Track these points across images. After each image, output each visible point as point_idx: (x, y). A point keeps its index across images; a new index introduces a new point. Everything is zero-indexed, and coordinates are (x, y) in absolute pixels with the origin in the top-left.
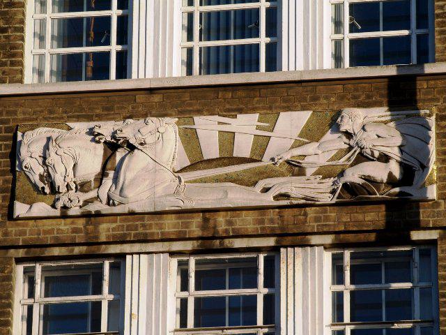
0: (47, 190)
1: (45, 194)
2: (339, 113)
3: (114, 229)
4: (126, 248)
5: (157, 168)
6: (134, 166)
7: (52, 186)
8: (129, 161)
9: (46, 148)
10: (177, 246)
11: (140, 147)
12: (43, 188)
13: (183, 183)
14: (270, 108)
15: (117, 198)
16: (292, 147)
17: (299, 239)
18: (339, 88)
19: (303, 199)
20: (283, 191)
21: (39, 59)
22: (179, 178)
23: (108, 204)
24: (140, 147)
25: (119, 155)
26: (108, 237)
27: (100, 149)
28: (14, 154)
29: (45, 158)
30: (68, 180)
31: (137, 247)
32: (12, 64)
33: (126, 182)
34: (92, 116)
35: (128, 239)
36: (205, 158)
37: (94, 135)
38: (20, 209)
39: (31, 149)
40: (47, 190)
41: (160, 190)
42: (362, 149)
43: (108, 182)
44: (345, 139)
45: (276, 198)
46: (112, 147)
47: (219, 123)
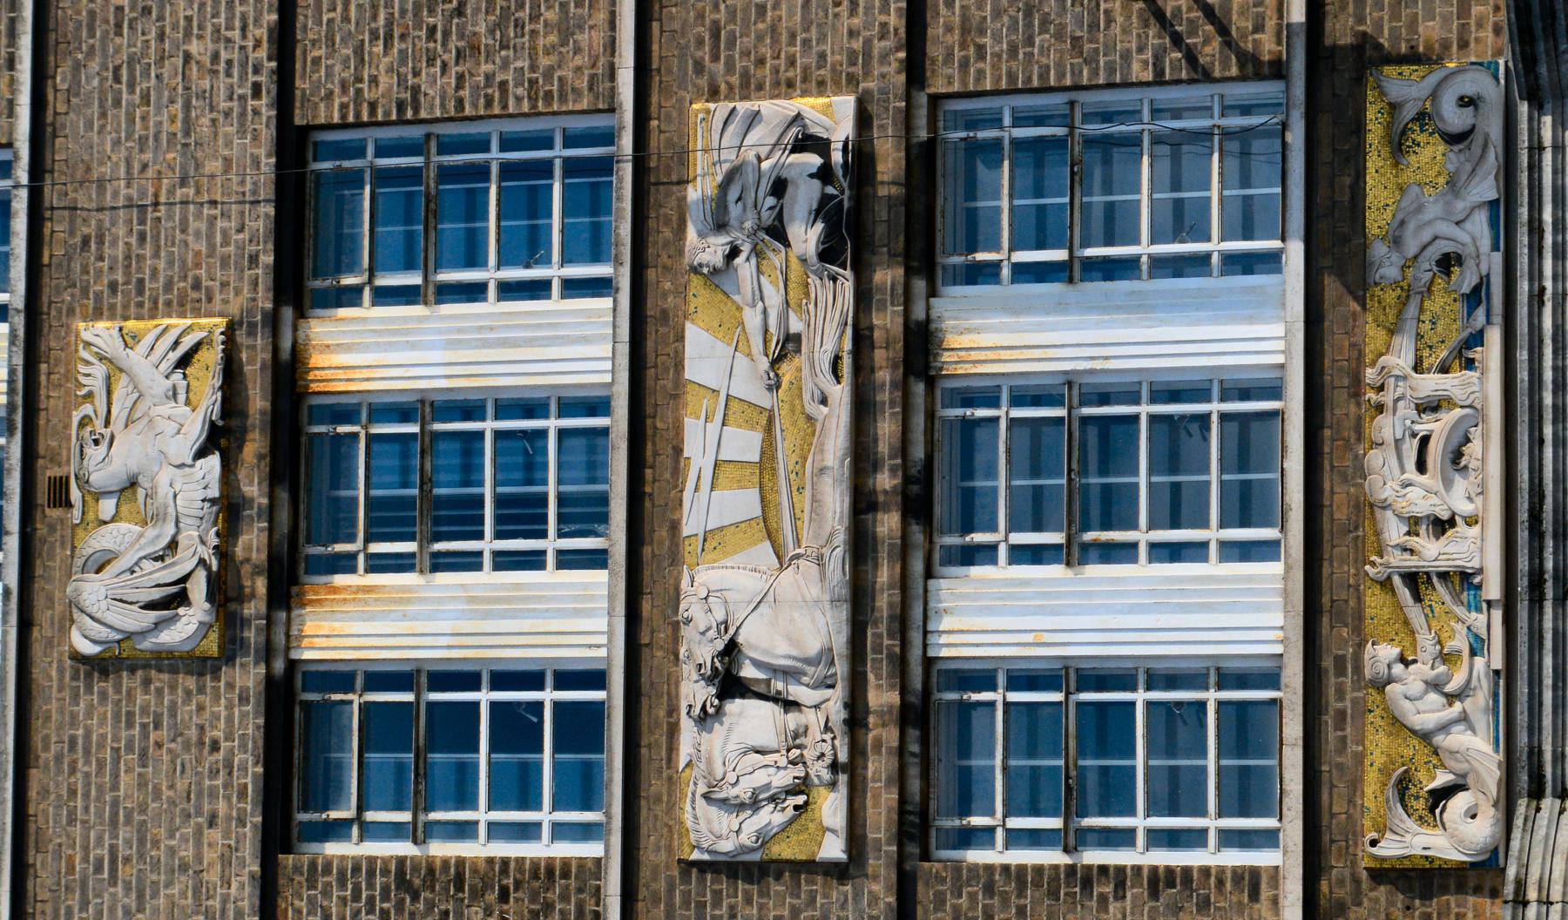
0: (801, 799)
1: (806, 803)
2: (695, 270)
3: (878, 677)
4: (915, 653)
5: (767, 594)
6: (767, 641)
7: (792, 791)
8: (756, 649)
9: (723, 803)
10: (918, 566)
11: (731, 631)
12: (796, 808)
13: (801, 551)
14: (676, 397)
15: (821, 671)
16: (749, 355)
17: (921, 344)
18: (1331, 286)
19: (843, 332)
20: (826, 367)
21: (558, 837)
22: (792, 559)
23: (832, 686)
24: (731, 631)
25: (748, 672)
26: (892, 687)
27: (735, 706)
28: (733, 869)
29: (741, 806)
30: (783, 762)
31: (916, 637)
32: (566, 875)
33: (794, 653)
34: (669, 723)
35: (897, 650)
36: (758, 512)
37: (705, 719)
38: (833, 849)
39: (725, 832)
40: (801, 799)
41: (814, 591)
42: (760, 228)
43: (797, 692)
44: (739, 261)
45: (838, 379)
46: (729, 685)
47: (696, 489)
